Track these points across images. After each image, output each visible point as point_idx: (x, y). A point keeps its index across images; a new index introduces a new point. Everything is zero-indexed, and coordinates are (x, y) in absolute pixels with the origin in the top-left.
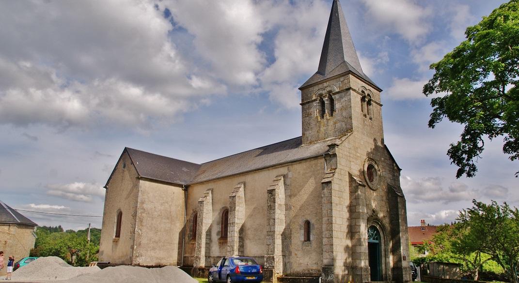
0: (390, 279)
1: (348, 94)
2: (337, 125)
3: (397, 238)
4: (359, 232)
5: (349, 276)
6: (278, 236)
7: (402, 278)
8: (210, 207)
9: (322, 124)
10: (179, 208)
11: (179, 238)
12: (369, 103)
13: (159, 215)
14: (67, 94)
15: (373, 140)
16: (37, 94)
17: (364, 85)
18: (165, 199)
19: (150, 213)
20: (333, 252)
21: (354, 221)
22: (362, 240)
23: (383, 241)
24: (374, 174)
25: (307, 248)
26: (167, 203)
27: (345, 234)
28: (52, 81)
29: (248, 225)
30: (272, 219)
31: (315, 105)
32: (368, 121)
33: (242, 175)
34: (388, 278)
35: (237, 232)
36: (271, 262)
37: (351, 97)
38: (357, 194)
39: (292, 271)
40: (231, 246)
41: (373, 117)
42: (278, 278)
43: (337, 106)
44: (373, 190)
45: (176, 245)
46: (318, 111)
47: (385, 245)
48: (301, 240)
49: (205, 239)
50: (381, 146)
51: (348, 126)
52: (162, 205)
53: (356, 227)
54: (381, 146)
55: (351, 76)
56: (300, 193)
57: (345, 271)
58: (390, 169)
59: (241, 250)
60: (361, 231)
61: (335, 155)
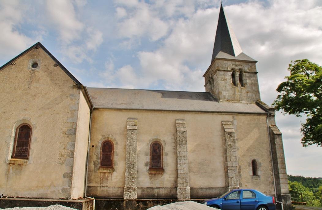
1: (255, 76)
2: (249, 94)
25: (257, 181)
30: (234, 156)
33: (181, 113)
40: (183, 178)
48: (251, 175)
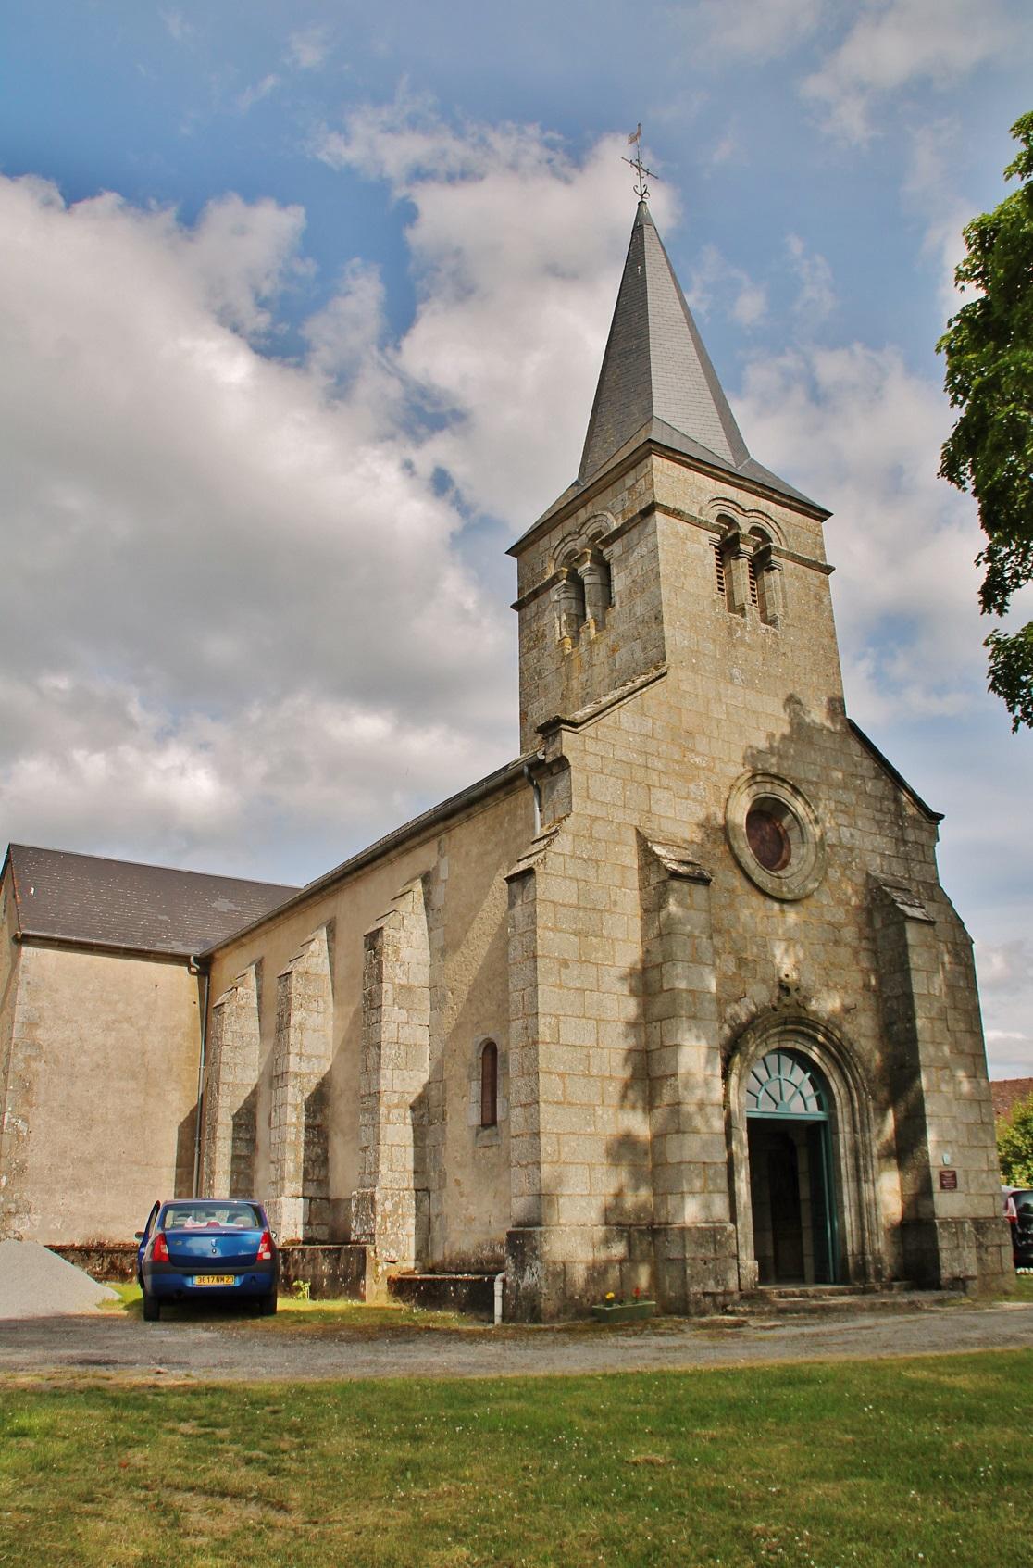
0: (879, 1273)
1: (649, 529)
3: (911, 1095)
4: (675, 1075)
5: (634, 1269)
6: (395, 1111)
7: (937, 1267)
8: (252, 1026)
9: (576, 663)
10: (178, 1038)
11: (181, 1145)
12: (761, 563)
13: (98, 1066)
14: (175, 756)
15: (780, 702)
16: (94, 765)
17: (731, 492)
18: (120, 1006)
19: (62, 1059)
20: (538, 1164)
21: (655, 1029)
22: (690, 1108)
23: (842, 1114)
24: (794, 836)
25: (489, 1153)
26: (129, 1020)
27: (614, 1090)
28: (131, 724)
29: (340, 1081)
31: (556, 597)
32: (755, 629)
34: (871, 1270)
35: (296, 1107)
36: (367, 1215)
37: (659, 539)
38: (663, 914)
39: (447, 1253)
41: (786, 615)
42: (391, 1282)
43: (619, 583)
44: (782, 901)
45: (165, 1170)
46: (564, 618)
47: (854, 1130)
48: (471, 1124)
49: (229, 1142)
50: (828, 724)
51: (653, 653)
52: (108, 1027)
53: (665, 1053)
54: (828, 724)
55: (656, 461)
56: (470, 935)
57: (607, 1242)
58: (878, 816)
59: (316, 1173)
60: (682, 1070)
61: (562, 763)
